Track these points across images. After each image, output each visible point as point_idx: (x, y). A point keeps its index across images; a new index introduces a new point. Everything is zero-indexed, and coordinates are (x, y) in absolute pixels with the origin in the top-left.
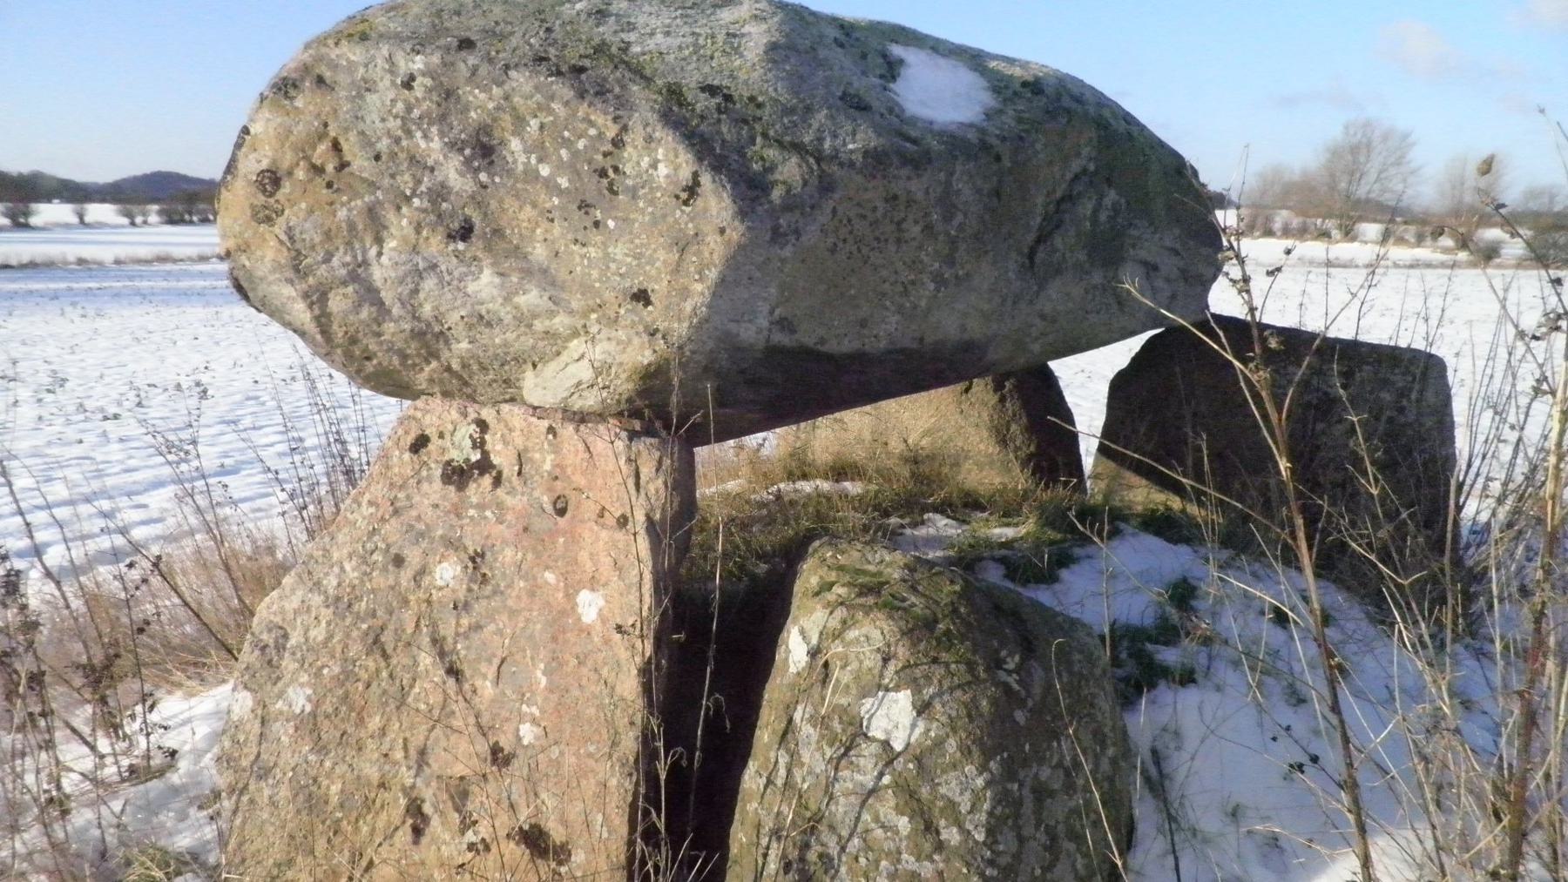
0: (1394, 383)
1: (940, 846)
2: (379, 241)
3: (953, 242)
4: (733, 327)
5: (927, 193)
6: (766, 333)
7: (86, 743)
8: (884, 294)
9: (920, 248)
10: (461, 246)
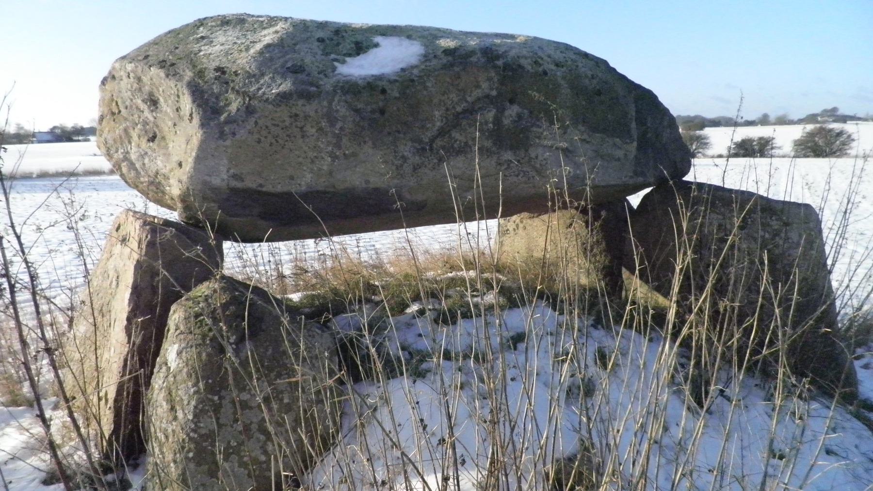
0: (771, 226)
1: (175, 418)
2: (130, 143)
3: (339, 137)
4: (207, 178)
5: (316, 112)
6: (226, 181)
7: (420, 474)
8: (301, 163)
9: (318, 139)
10: (151, 144)
